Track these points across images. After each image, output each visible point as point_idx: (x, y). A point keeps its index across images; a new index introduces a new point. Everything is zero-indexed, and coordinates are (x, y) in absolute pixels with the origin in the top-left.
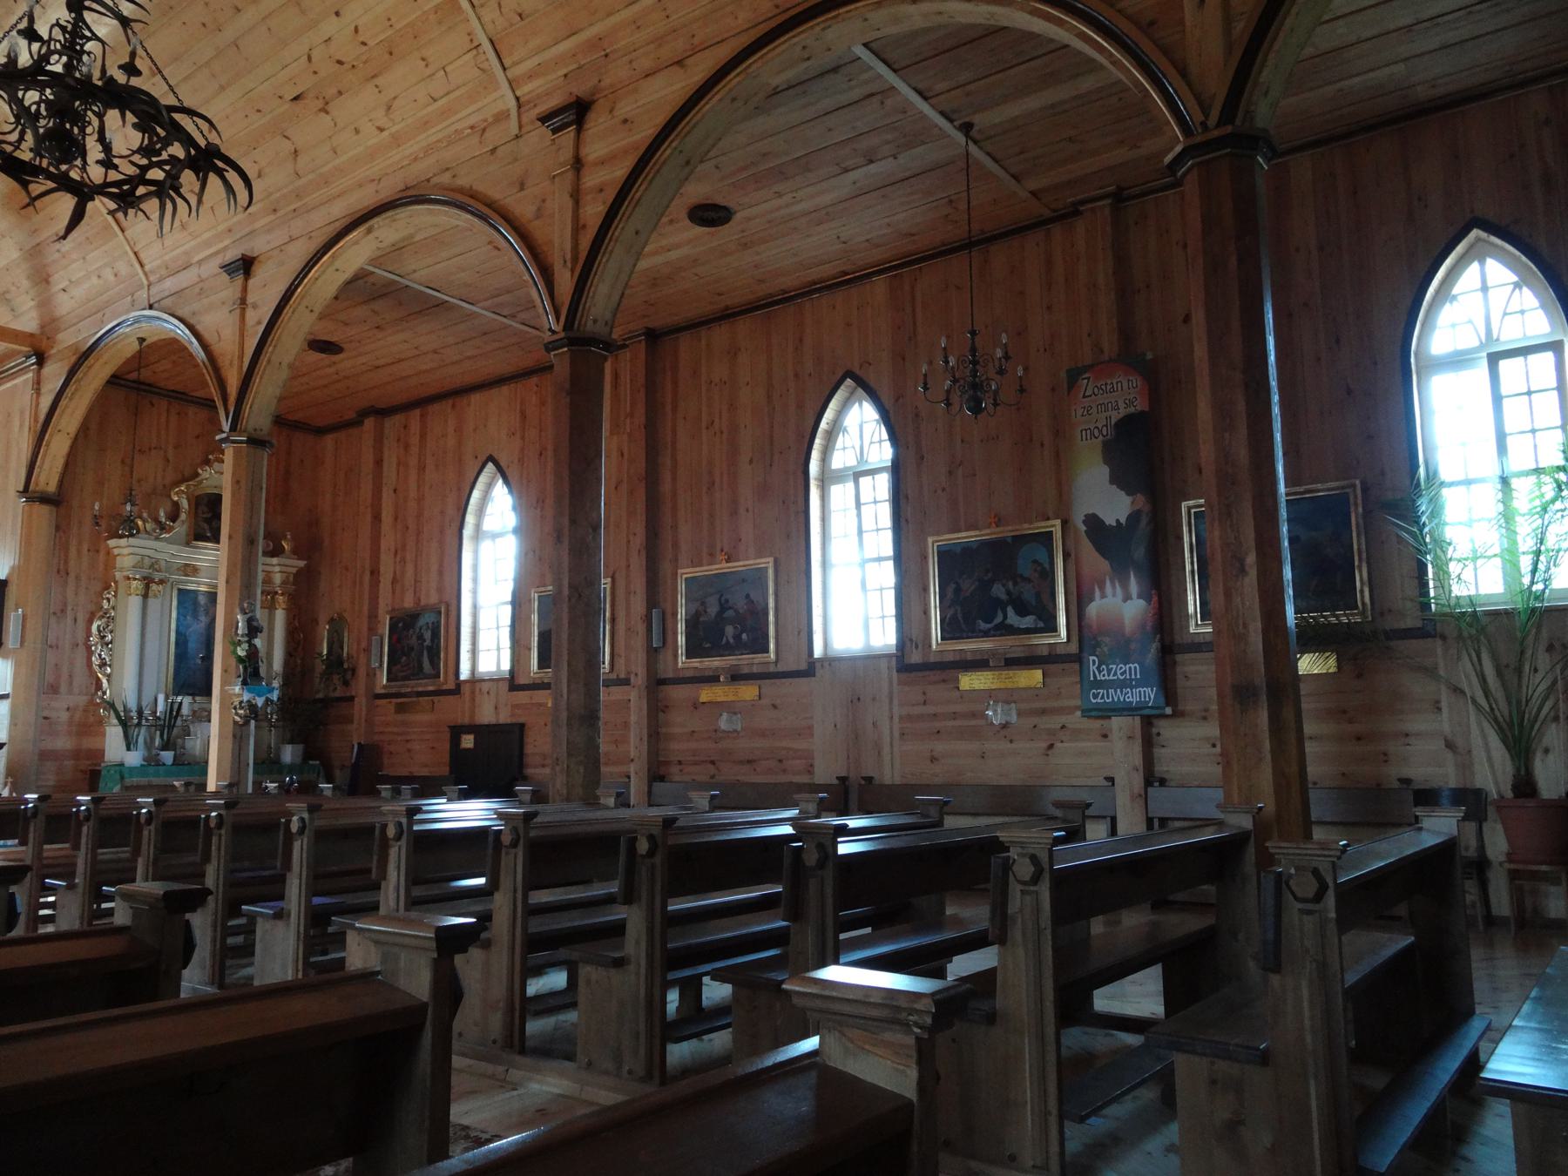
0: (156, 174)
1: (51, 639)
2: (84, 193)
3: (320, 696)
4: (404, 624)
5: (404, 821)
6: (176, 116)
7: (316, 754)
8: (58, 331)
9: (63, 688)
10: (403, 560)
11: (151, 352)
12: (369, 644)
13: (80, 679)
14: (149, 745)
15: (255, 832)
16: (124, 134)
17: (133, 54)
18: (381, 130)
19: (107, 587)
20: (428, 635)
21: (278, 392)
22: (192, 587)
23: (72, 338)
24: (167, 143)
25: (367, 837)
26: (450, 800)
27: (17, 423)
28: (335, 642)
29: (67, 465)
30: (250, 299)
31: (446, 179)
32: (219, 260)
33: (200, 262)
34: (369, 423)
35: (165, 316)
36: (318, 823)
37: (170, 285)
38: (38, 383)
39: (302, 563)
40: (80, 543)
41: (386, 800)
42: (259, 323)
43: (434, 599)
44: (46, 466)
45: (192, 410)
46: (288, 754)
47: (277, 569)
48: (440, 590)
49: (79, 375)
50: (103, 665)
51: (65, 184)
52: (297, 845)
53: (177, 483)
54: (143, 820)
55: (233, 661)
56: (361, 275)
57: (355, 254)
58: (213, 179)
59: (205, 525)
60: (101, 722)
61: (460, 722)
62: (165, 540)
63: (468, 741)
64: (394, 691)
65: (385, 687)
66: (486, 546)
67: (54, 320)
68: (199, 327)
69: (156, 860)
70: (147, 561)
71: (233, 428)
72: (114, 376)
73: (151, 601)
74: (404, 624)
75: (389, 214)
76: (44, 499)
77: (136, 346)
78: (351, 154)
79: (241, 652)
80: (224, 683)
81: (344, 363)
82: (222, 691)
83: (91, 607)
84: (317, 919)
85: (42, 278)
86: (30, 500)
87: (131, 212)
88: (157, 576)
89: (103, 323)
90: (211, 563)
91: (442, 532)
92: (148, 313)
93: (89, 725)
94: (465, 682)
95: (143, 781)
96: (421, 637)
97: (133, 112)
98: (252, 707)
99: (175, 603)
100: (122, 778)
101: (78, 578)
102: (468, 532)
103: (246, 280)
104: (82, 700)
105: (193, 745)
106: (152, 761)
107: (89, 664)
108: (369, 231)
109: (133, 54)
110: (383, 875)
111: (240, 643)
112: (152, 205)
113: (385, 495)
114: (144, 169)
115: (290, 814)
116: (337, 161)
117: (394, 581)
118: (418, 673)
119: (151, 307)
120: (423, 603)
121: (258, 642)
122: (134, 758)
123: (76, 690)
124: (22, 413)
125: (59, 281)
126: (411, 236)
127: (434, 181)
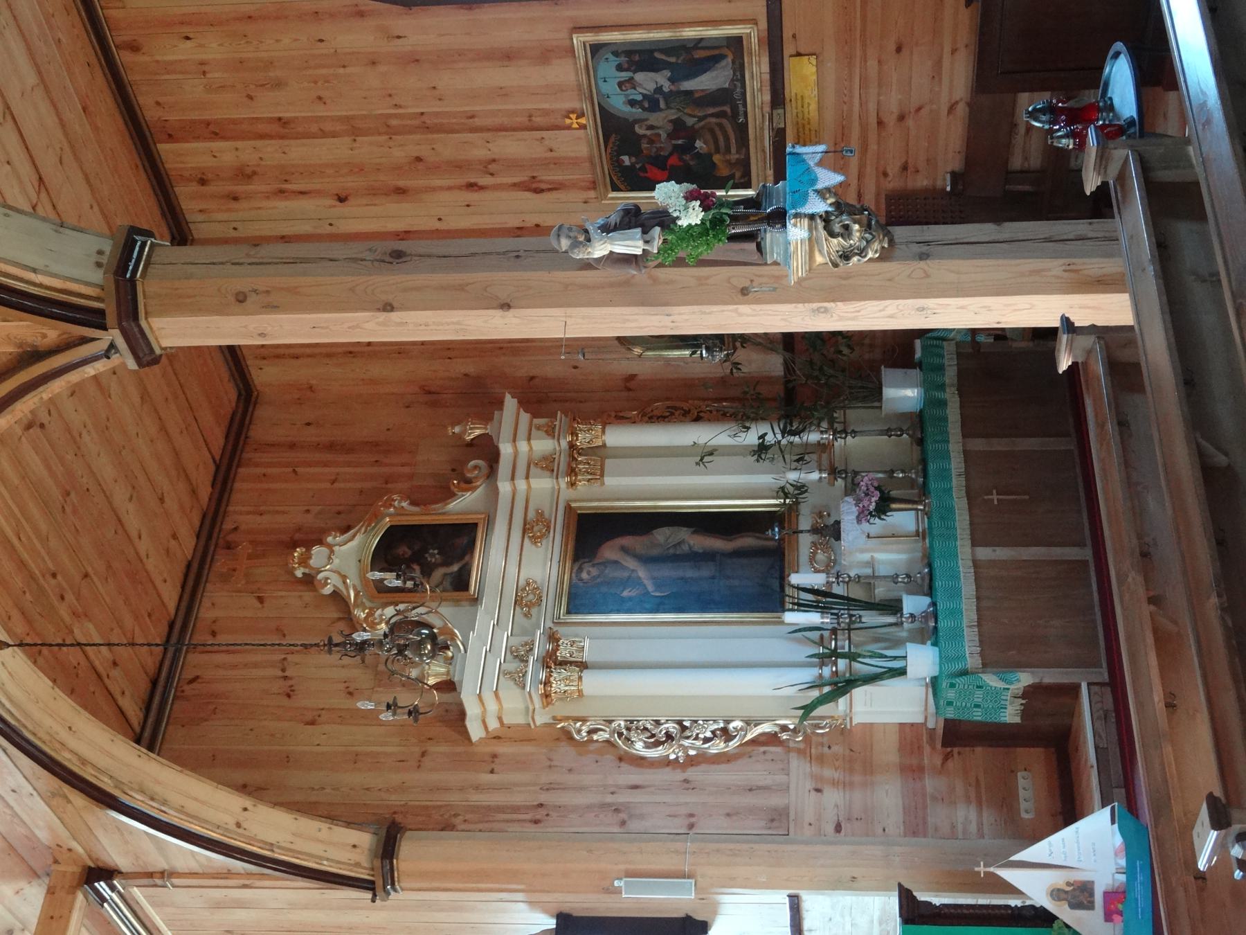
1: (679, 825)
9: (776, 801)
10: (488, 165)
13: (755, 771)
38: (150, 875)
39: (510, 403)
40: (478, 788)
43: (564, 73)
44: (316, 849)
45: (206, 613)
47: (523, 446)
49: (106, 784)
50: (726, 734)
60: (842, 732)
70: (513, 666)
73: (586, 656)
76: (387, 850)
80: (780, 293)
83: (610, 758)
91: (414, 60)
93: (852, 754)
96: (651, 103)
100: (964, 673)
101: (548, 788)
104: (799, 769)
106: (928, 631)
118: (729, 101)
122: (922, 660)
123: (781, 778)
124: (219, 906)
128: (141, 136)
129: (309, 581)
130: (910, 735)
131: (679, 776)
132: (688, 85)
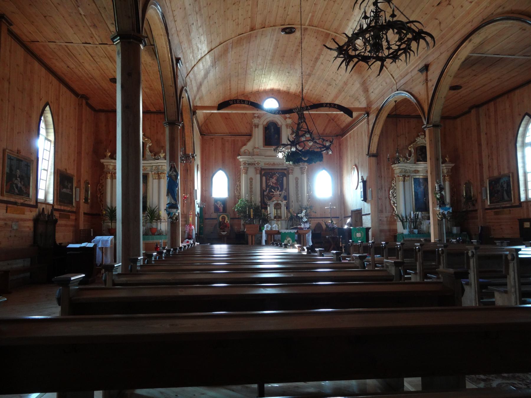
0: (404, 46)
2: (382, 60)
3: (464, 210)
4: (494, 182)
5: (515, 254)
6: (409, 25)
7: (464, 230)
8: (372, 105)
9: (384, 211)
10: (492, 159)
11: (398, 104)
12: (481, 189)
13: (388, 208)
14: (410, 228)
15: (456, 257)
16: (392, 36)
17: (393, 11)
18: (471, 2)
19: (393, 180)
20: (505, 186)
21: (442, 108)
22: (418, 177)
23: (375, 106)
24: (406, 35)
25: (501, 260)
26: (526, 247)
27: (364, 135)
28: (468, 191)
29: (378, 144)
30: (429, 78)
31: (500, 10)
32: (417, 69)
33: (411, 71)
34: (473, 111)
35: (402, 92)
36: (478, 253)
37: (403, 81)
39: (453, 165)
40: (384, 167)
41: (498, 246)
42: (433, 85)
43: (506, 172)
46: (455, 230)
47: (445, 168)
48: (509, 168)
49: (379, 117)
50: (394, 203)
51: (378, 58)
52: (471, 261)
53: (410, 144)
54: (440, 253)
55: (436, 199)
56: (468, 59)
57: (465, 51)
58: (422, 41)
59: (421, 155)
60: (395, 221)
61: (522, 217)
62: (409, 163)
63: (527, 225)
64: (492, 207)
65: (489, 206)
66: (528, 149)
67: (371, 102)
68: (413, 93)
69: (422, 263)
71: (428, 123)
72: (388, 115)
73: (406, 182)
74: (494, 182)
75: (477, 32)
77: (394, 104)
78: (461, 15)
79: (438, 196)
80: (433, 207)
81: (463, 92)
82: (433, 210)
84: (482, 287)
85: (366, 90)
86: (370, 156)
87: (397, 60)
88: (407, 175)
89: (384, 99)
90: (423, 168)
92: (397, 92)
93: (392, 222)
94: (523, 202)
95: (410, 239)
96: (502, 186)
97: (396, 29)
98: (443, 214)
99: (413, 183)
101: (384, 178)
102: (519, 144)
103: (427, 72)
105: (424, 227)
106: (411, 232)
107: (390, 203)
108: (470, 41)
109: (393, 11)
110: (508, 273)
111: (437, 193)
112: (403, 57)
113: (482, 136)
114: (399, 46)
115: (468, 250)
116: (456, 20)
117: (489, 167)
118: (503, 199)
119: (397, 90)
120: (502, 173)
121: (443, 193)
122: (406, 232)
125: (371, 90)
126: (487, 37)
127: (495, 13)
128: (494, 99)
129: (418, 136)
130: (396, 230)
131: (387, 197)
132: (505, 193)
